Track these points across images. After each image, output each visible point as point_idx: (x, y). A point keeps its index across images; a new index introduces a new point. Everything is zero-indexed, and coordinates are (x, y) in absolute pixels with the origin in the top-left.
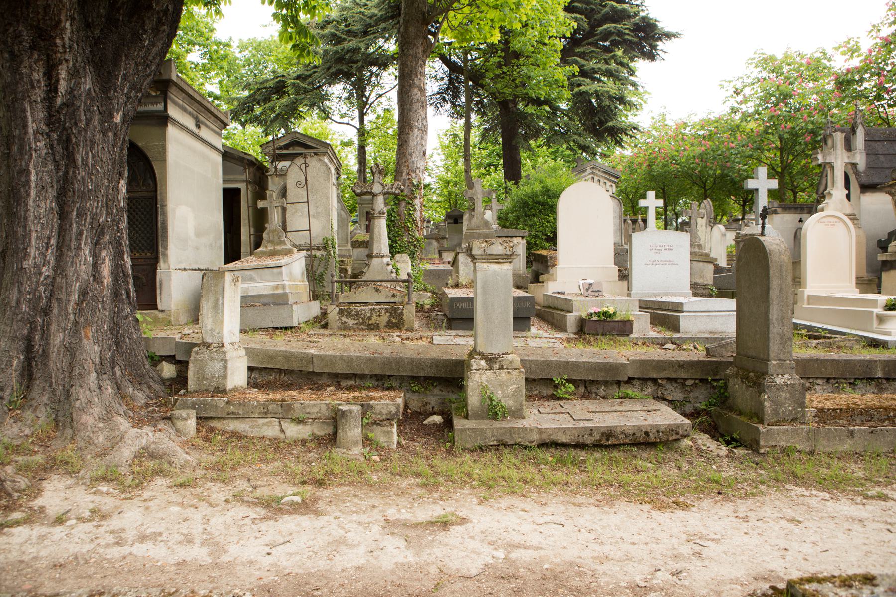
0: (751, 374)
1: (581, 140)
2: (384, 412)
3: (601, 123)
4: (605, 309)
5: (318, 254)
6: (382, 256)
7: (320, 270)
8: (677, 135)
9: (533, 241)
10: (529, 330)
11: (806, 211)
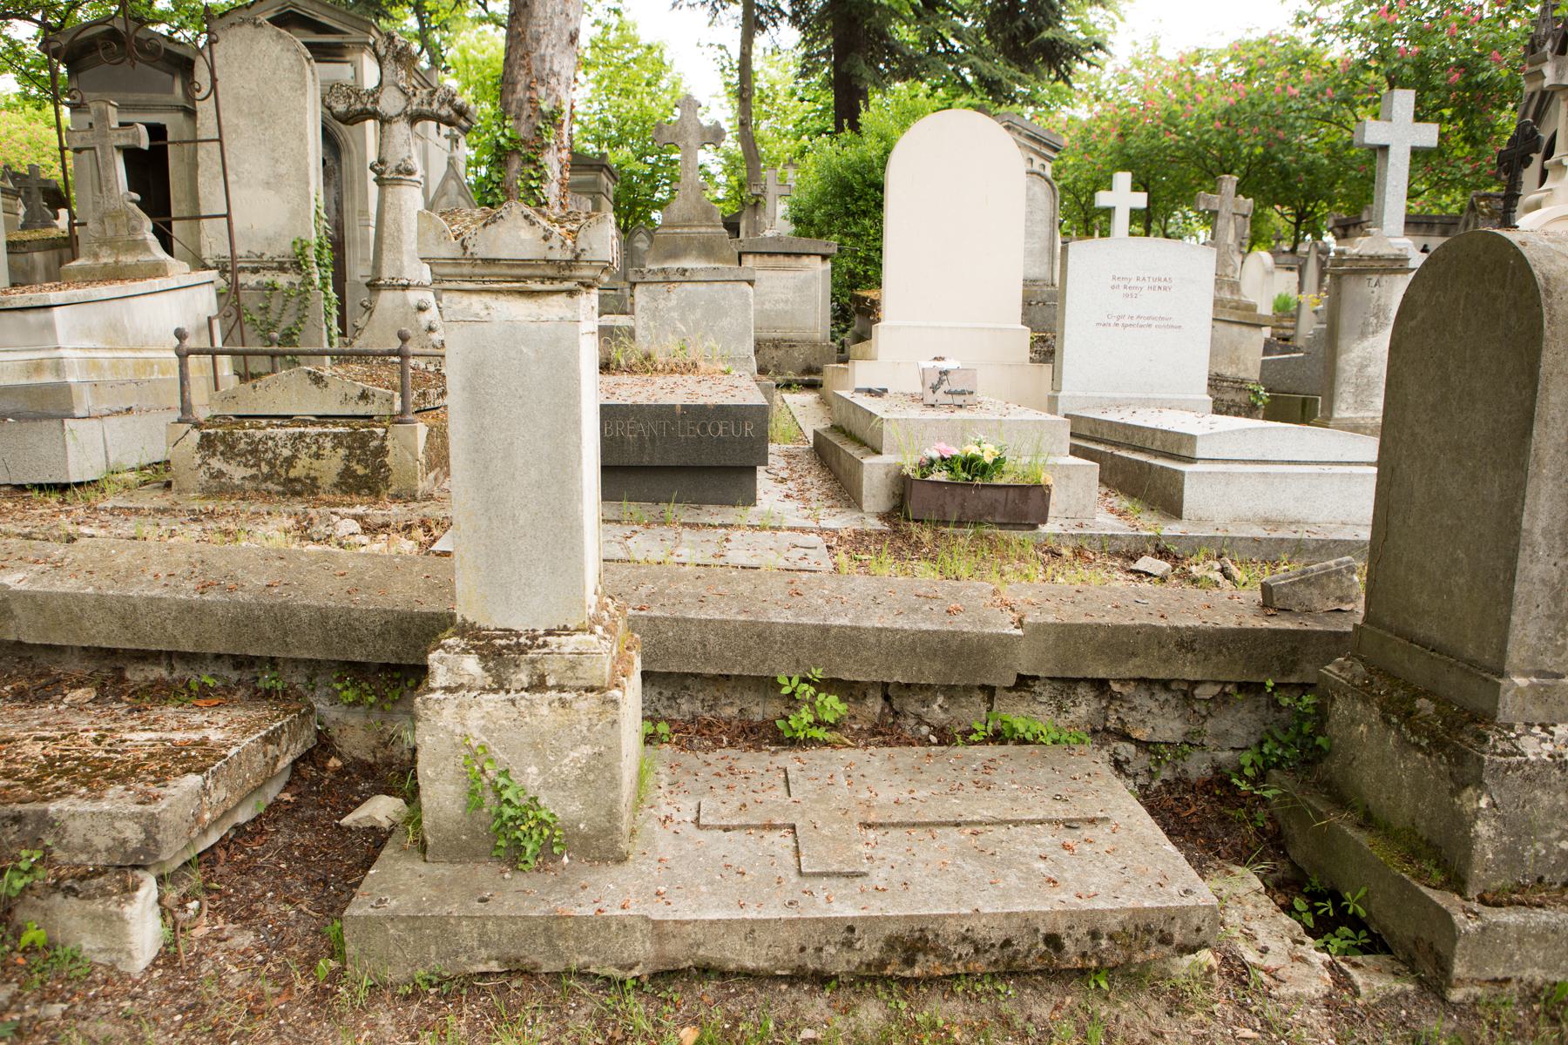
0: (1421, 703)
1: (985, 68)
2: (101, 842)
3: (1030, 32)
4: (973, 450)
5: (282, 280)
6: (406, 287)
7: (287, 321)
8: (1180, 75)
9: (860, 269)
10: (751, 500)
11: (1437, 230)
